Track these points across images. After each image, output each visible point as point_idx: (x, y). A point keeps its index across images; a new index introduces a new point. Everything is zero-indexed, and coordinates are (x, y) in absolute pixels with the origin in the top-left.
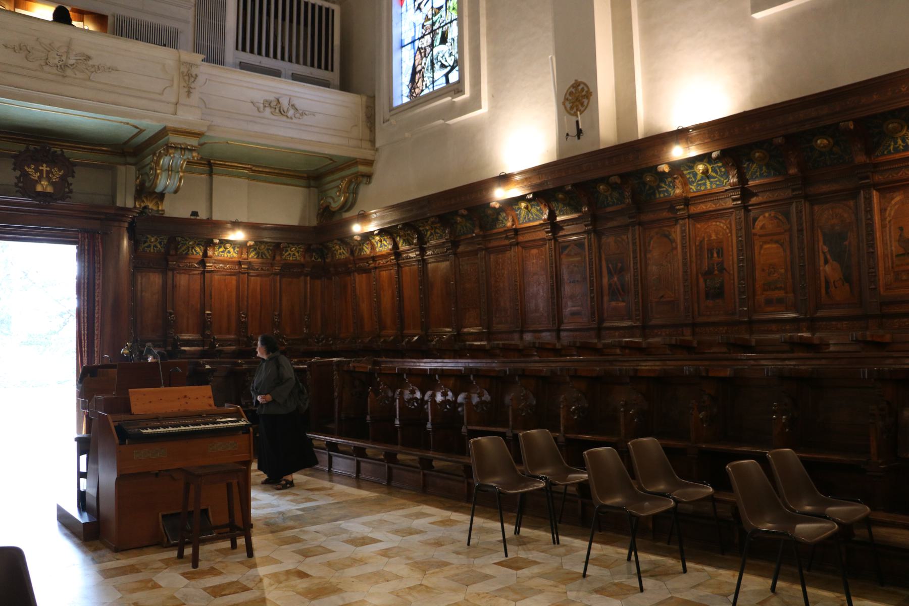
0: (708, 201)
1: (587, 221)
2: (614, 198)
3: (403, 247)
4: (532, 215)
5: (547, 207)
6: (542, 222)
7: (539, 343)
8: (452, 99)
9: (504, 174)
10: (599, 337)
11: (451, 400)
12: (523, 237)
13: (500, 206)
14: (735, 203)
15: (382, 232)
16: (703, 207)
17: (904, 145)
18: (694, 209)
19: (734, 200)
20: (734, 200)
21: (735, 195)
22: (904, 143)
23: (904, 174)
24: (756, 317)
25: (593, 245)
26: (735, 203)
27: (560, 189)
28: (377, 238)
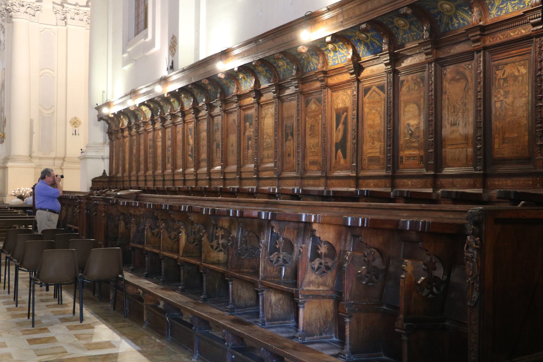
0: (497, 31)
1: (537, 18)
2: (460, 19)
3: (365, 56)
4: (313, 64)
5: (350, 46)
6: (423, 41)
7: (367, 191)
8: (145, 39)
9: (310, 13)
10: (240, 184)
11: (441, 278)
12: (493, 38)
13: (302, 53)
14: (535, 28)
15: (336, 38)
16: (500, 37)
17: (458, 22)
18: (490, 41)
19: (534, 25)
20: (534, 25)
21: (535, 18)
22: (457, 21)
23: (498, 39)
24: (362, 173)
25: (329, 103)
26: (535, 28)
27: (356, 28)
28: (330, 46)
